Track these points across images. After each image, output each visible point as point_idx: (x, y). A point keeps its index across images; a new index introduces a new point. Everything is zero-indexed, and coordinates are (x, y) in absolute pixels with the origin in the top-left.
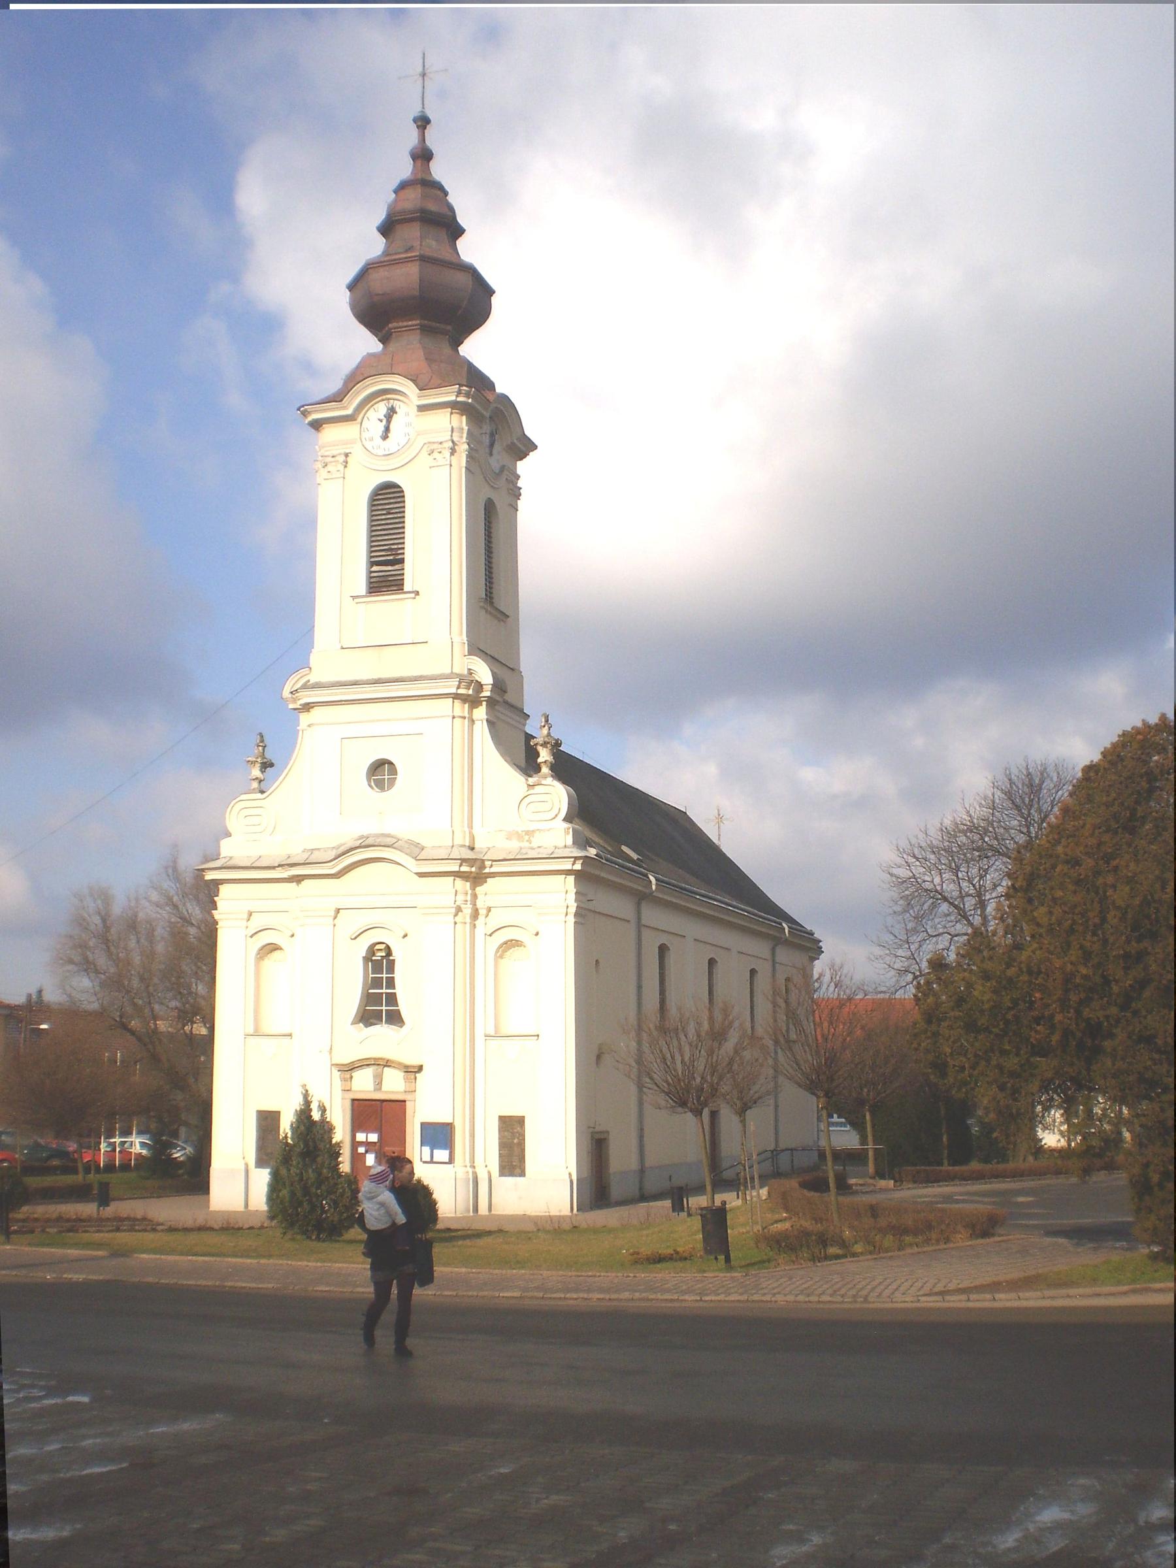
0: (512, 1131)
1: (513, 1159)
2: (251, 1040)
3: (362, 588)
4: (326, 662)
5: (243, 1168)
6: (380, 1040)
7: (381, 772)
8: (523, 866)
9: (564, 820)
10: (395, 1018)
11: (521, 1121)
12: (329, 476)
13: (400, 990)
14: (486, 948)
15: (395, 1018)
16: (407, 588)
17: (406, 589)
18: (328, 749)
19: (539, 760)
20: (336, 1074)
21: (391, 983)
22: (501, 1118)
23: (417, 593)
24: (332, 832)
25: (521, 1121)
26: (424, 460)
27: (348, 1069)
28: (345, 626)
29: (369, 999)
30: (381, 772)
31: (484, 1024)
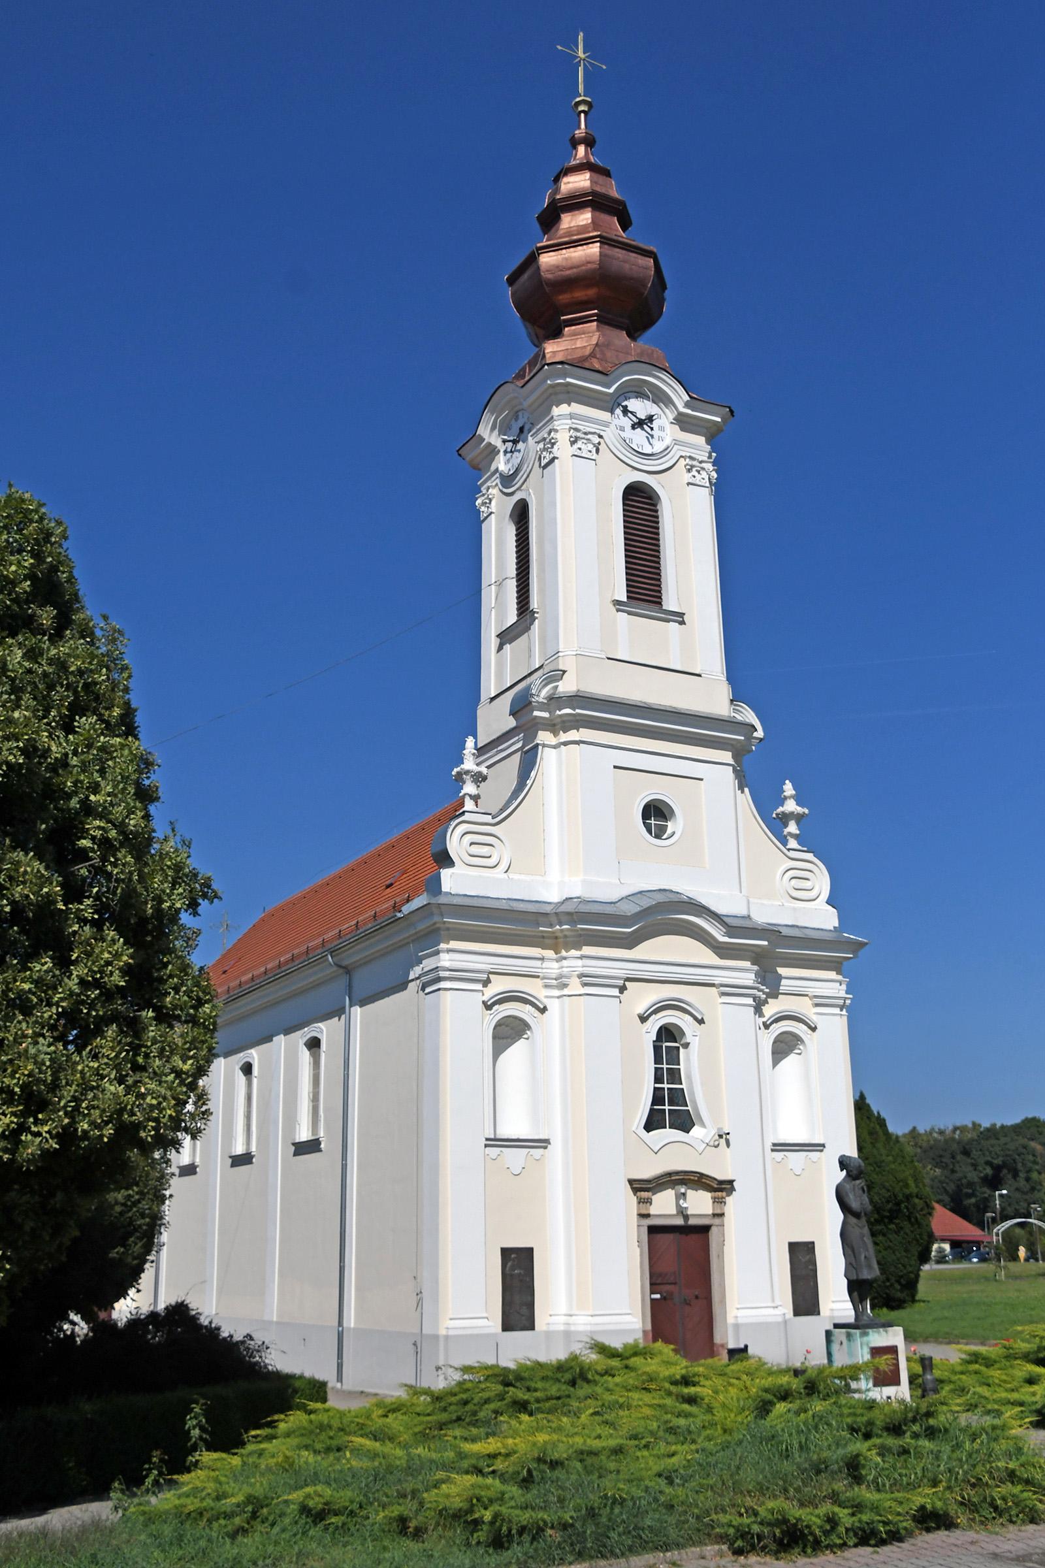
6: (671, 1150)
15: (684, 1122)
22: (530, 1251)
27: (642, 1188)
28: (582, 626)
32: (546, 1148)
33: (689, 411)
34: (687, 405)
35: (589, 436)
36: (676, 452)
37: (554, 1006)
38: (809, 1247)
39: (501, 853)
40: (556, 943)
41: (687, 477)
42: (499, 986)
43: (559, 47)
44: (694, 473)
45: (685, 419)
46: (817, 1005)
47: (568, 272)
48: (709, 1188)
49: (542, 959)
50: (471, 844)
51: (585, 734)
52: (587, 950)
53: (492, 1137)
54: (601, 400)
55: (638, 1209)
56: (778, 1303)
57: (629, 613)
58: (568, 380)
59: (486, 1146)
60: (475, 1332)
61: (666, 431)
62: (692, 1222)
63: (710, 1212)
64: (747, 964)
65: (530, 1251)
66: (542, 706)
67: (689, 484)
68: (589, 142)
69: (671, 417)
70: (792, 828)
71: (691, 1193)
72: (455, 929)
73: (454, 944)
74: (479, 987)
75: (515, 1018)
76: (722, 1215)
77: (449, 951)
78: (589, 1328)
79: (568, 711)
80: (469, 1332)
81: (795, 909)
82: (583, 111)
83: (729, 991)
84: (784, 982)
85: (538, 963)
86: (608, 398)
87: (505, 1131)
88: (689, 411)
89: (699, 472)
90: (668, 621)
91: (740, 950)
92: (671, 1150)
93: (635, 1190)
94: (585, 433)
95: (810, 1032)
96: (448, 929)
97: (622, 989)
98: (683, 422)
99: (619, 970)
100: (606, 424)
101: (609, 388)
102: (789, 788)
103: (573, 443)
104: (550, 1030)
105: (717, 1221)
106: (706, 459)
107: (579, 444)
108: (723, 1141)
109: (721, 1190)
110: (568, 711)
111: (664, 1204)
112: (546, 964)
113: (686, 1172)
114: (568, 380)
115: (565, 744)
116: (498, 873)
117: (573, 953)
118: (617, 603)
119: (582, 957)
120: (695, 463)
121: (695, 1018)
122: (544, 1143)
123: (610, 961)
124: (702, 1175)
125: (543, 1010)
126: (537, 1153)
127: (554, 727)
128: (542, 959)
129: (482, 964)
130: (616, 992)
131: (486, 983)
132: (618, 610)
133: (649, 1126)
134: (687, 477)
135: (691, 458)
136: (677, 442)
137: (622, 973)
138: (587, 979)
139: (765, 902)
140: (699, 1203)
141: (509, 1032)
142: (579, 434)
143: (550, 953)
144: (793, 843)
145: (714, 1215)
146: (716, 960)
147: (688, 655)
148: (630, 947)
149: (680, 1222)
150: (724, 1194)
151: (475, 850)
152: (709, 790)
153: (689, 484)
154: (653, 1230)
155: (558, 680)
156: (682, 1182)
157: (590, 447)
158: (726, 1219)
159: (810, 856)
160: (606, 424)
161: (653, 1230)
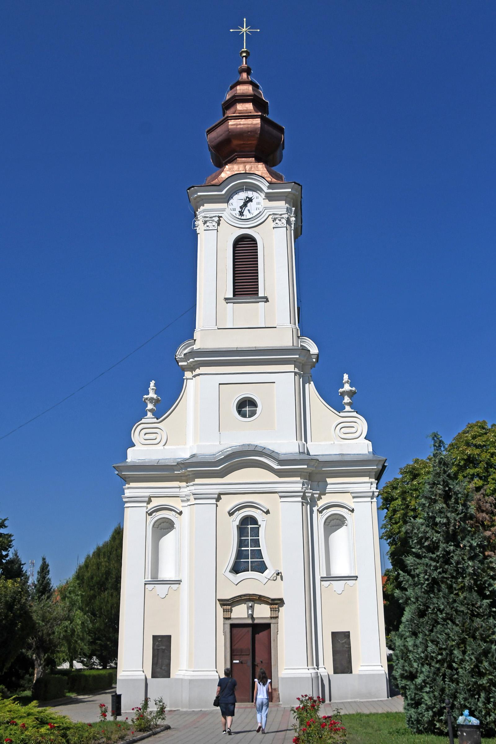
0: (342, 643)
1: (343, 662)
2: (149, 587)
3: (230, 294)
4: (205, 337)
5: (144, 678)
6: (251, 582)
7: (246, 406)
8: (347, 467)
9: (366, 438)
10: (261, 568)
11: (347, 635)
12: (277, 226)
13: (263, 547)
14: (319, 521)
15: (261, 568)
16: (261, 294)
17: (260, 295)
18: (201, 391)
19: (148, 408)
20: (220, 610)
21: (256, 543)
22: (169, 637)
23: (267, 301)
24: (214, 446)
25: (347, 635)
26: (270, 223)
27: (227, 604)
28: (216, 315)
29: (240, 554)
30: (246, 406)
31: (321, 572)
32: (180, 584)
33: (271, 191)
34: (269, 188)
35: (213, 218)
36: (267, 213)
37: (186, 511)
38: (167, 639)
39: (162, 435)
40: (188, 479)
41: (273, 225)
42: (155, 503)
43: (259, 30)
44: (277, 221)
45: (270, 195)
46: (354, 497)
47: (219, 139)
48: (267, 603)
49: (180, 487)
50: (145, 434)
51: (203, 370)
52: (197, 481)
53: (325, 576)
54: (222, 199)
55: (224, 615)
56: (309, 667)
57: (234, 303)
58: (199, 194)
59: (321, 581)
60: (134, 678)
61: (259, 203)
62: (256, 621)
63: (269, 616)
64: (298, 479)
65: (169, 637)
66: (182, 360)
67: (274, 228)
68: (248, 71)
69: (263, 195)
70: (347, 399)
71: (257, 606)
72: (132, 477)
73: (132, 485)
74: (145, 504)
75: (332, 515)
76: (278, 617)
77: (129, 488)
78: (189, 678)
79: (191, 360)
80: (130, 678)
81: (341, 445)
82: (244, 56)
83: (284, 495)
84: (329, 486)
85: (177, 490)
86: (224, 197)
87: (336, 571)
88: (271, 191)
89: (280, 220)
90: (258, 302)
91: (295, 472)
92: (251, 582)
93: (222, 605)
94: (211, 218)
95: (350, 513)
96: (129, 477)
97: (218, 499)
98: (270, 197)
99: (216, 490)
100: (224, 210)
101: (222, 191)
102: (346, 377)
103: (204, 224)
104: (182, 524)
105: (273, 621)
106: (285, 212)
107: (208, 224)
108: (279, 577)
109: (276, 604)
110: (191, 360)
111: (240, 613)
112: (182, 490)
113: (240, 596)
114: (199, 194)
115: (199, 375)
116: (160, 447)
117: (192, 483)
118: (226, 299)
119: (194, 485)
120: (207, 219)
121: (349, 510)
122: (178, 582)
123: (209, 486)
124: (260, 596)
125: (180, 513)
126: (175, 587)
127: (192, 368)
128: (180, 487)
129: (147, 493)
130: (214, 501)
131: (149, 501)
132: (227, 303)
133: (236, 569)
134: (273, 225)
135: (273, 214)
136: (266, 208)
137: (217, 491)
138: (197, 496)
139: (321, 443)
140: (262, 612)
141: (164, 527)
142: (207, 219)
143: (184, 484)
144: (348, 408)
145: (271, 618)
146: (276, 479)
147: (275, 316)
148: (222, 477)
149: (250, 621)
150: (277, 606)
151: (147, 436)
152: (279, 388)
153: (274, 228)
154: (233, 626)
155: (193, 345)
156: (250, 600)
157: (214, 223)
158: (280, 620)
159: (355, 414)
160: (224, 210)
161: (233, 626)
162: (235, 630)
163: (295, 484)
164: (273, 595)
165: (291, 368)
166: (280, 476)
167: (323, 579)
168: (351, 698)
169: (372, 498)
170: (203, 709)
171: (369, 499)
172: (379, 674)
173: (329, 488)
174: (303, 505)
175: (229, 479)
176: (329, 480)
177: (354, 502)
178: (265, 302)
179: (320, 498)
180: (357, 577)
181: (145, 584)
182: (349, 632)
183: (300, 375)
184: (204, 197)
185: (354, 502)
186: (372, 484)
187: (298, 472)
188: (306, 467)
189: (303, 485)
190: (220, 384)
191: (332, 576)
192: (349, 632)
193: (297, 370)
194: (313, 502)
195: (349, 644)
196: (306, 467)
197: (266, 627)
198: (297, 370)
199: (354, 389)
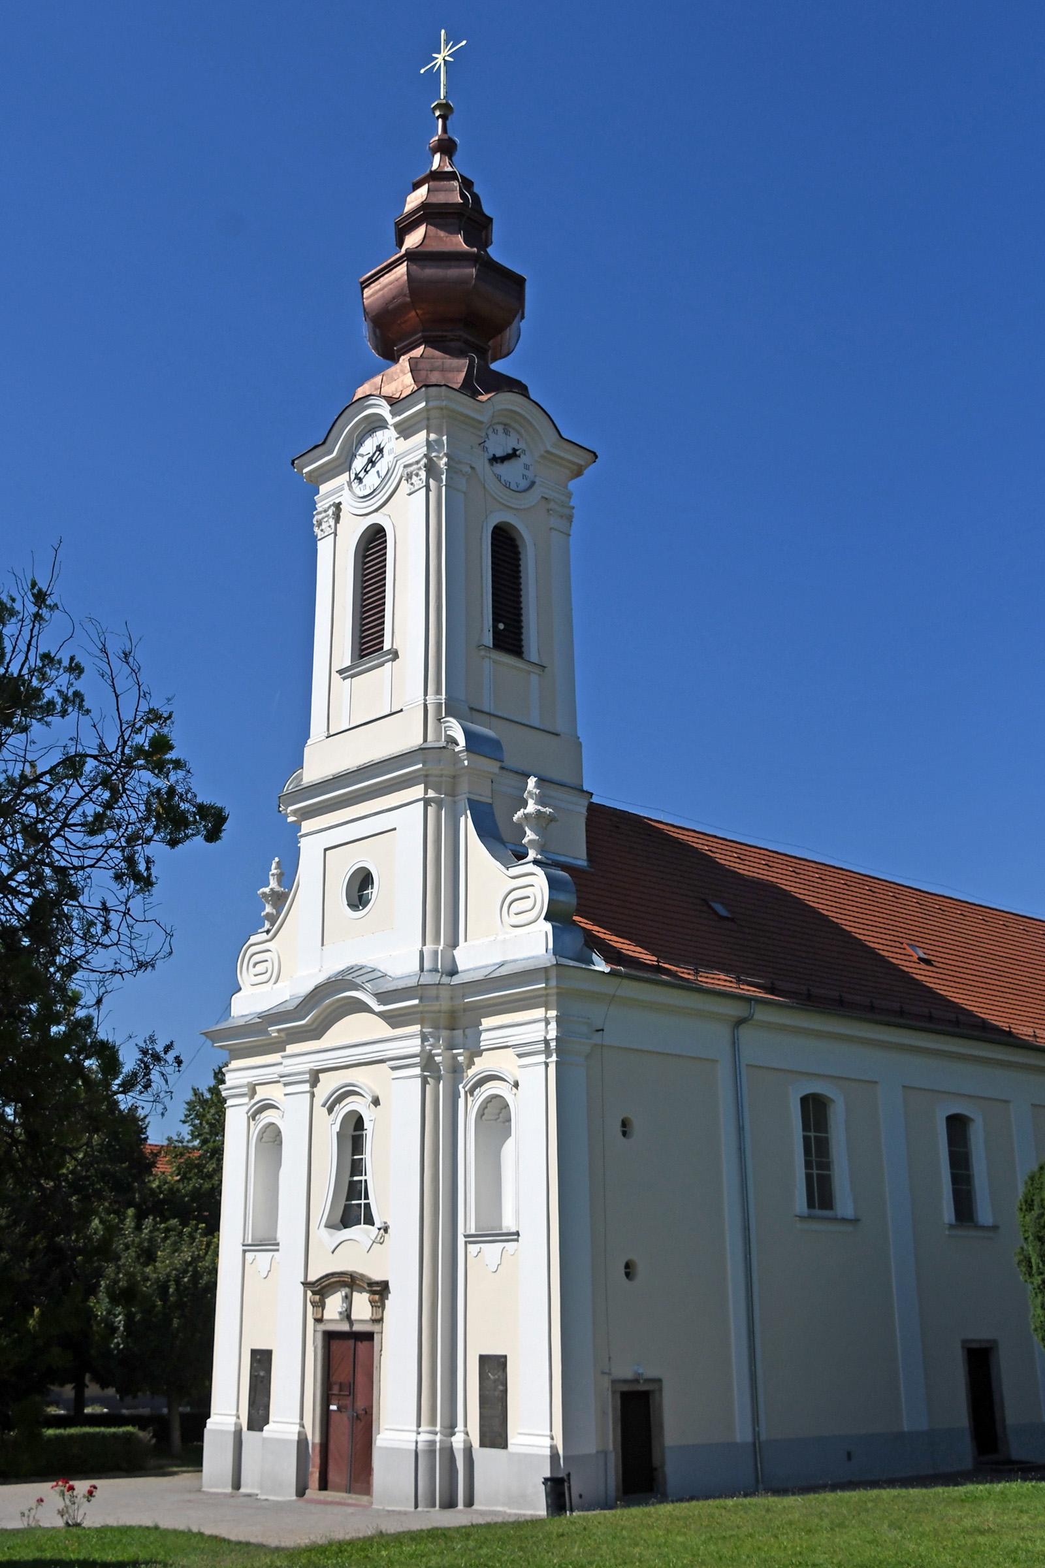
11: (269, 1353)
16: (387, 646)
25: (269, 1353)
27: (320, 1289)
31: (467, 1223)
52: (291, 1049)
57: (352, 676)
67: (410, 494)
84: (484, 1036)
86: (342, 460)
88: (398, 419)
90: (382, 664)
91: (400, 1015)
92: (354, 1251)
132: (344, 679)
148: (318, 1036)
149: (345, 1327)
162: (336, 1345)
163: (409, 1041)
164: (377, 1277)
165: (418, 791)
166: (394, 1026)
167: (471, 1239)
168: (504, 1504)
169: (548, 1056)
170: (271, 1498)
171: (542, 1058)
172: (538, 1455)
173: (486, 1039)
174: (425, 1082)
175: (332, 1037)
176: (486, 1022)
177: (520, 1067)
178: (393, 660)
179: (471, 1063)
180: (517, 1234)
181: (245, 1251)
182: (505, 1357)
183: (439, 803)
184: (315, 474)
185: (520, 1067)
186: (547, 1023)
187: (414, 1013)
188: (416, 1002)
189: (424, 1038)
190: (326, 850)
191: (504, 1231)
192: (505, 1357)
193: (431, 794)
194: (457, 1071)
195: (505, 1384)
196: (416, 1002)
197: (369, 1337)
198: (431, 794)
199: (548, 810)
